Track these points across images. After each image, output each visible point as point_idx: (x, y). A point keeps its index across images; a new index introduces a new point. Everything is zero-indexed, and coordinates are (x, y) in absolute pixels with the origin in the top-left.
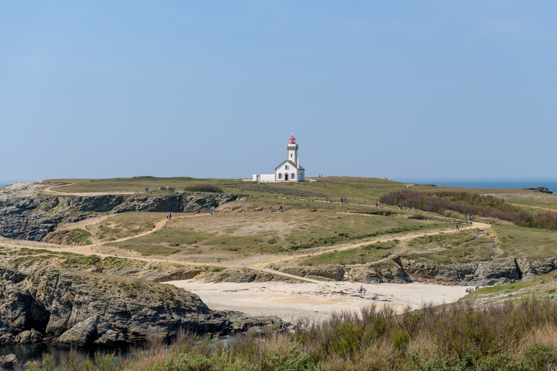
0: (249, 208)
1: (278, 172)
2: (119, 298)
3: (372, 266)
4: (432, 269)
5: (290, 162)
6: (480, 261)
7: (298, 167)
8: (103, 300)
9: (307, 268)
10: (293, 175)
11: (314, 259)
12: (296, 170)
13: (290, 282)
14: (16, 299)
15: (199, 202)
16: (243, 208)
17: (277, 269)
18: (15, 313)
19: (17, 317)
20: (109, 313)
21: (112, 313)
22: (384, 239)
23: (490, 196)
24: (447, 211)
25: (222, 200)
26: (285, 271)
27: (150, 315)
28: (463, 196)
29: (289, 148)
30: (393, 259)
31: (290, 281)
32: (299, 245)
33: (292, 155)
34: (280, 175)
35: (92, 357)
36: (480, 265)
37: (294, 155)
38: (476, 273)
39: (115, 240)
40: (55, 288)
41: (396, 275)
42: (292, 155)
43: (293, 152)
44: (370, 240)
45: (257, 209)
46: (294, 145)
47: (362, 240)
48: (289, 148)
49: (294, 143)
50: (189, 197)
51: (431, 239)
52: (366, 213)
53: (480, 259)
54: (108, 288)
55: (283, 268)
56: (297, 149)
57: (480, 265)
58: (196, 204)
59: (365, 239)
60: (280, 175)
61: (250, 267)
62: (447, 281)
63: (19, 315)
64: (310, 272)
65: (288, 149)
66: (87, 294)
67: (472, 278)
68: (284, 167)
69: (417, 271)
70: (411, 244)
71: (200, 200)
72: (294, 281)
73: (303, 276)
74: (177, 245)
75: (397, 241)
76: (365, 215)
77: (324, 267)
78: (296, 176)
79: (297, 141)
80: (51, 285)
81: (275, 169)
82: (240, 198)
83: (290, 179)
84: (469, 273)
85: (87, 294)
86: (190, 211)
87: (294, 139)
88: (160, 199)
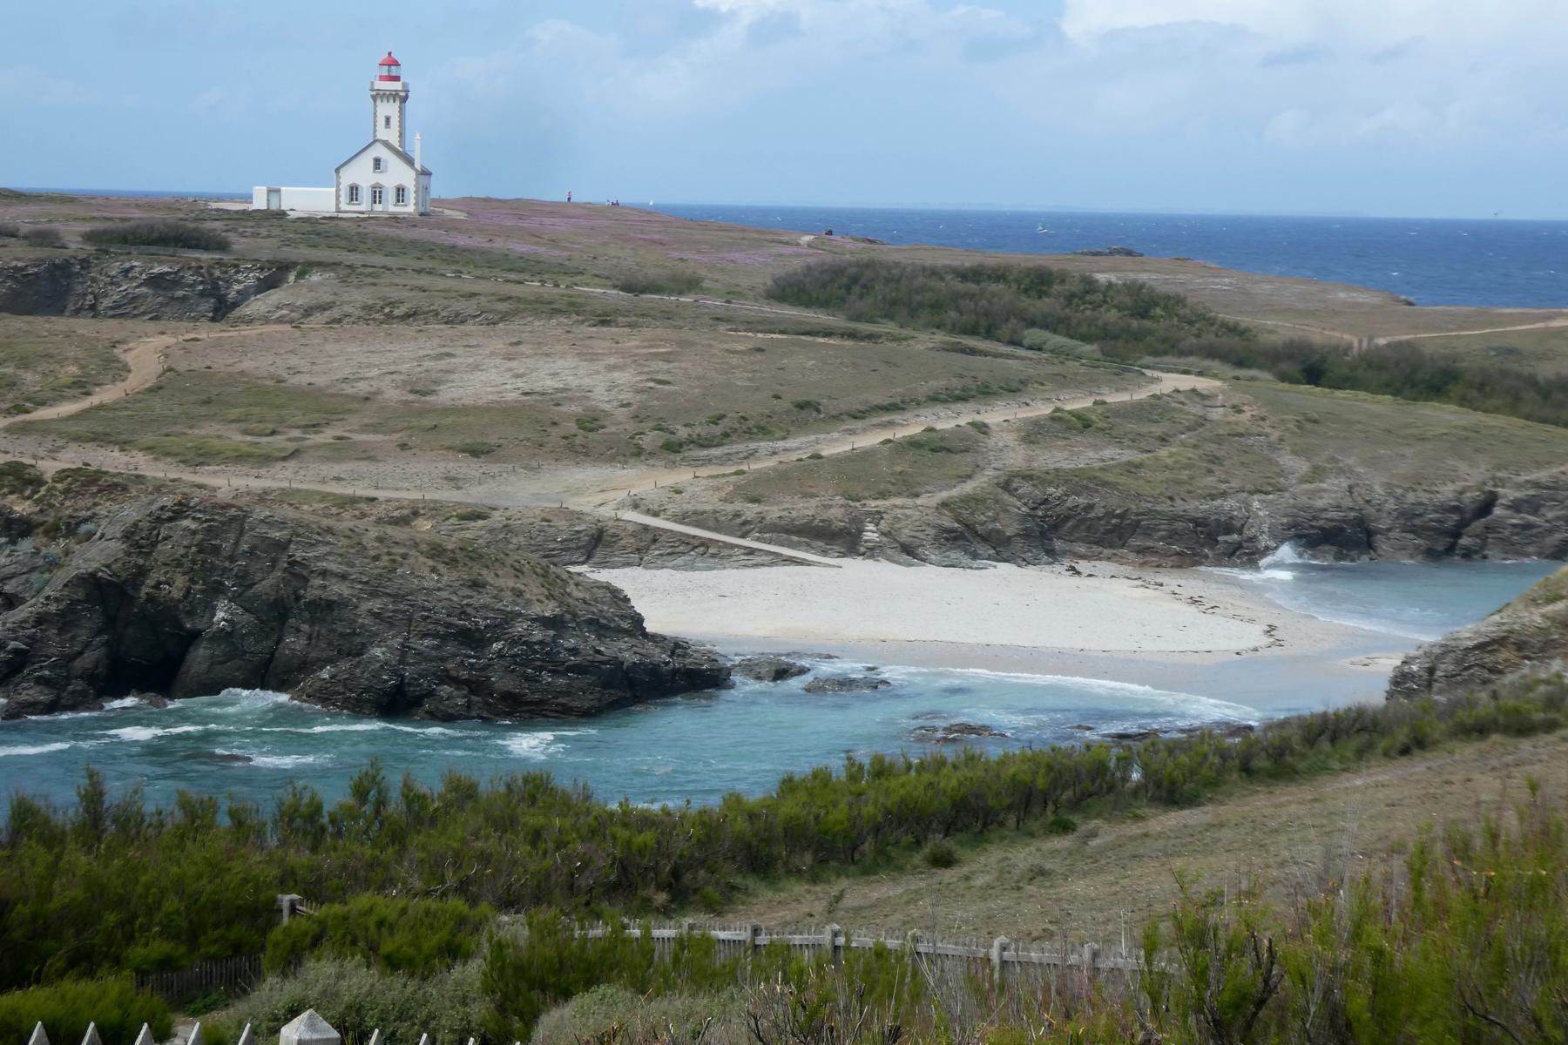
0: (368, 308)
1: (349, 177)
2: (439, 589)
3: (944, 505)
4: (1117, 516)
5: (386, 144)
6: (1251, 493)
7: (417, 166)
8: (395, 596)
9: (751, 511)
10: (400, 192)
11: (762, 479)
12: (413, 174)
13: (713, 556)
14: (81, 595)
15: (156, 281)
16: (348, 309)
17: (656, 514)
18: (73, 638)
19: (80, 653)
20: (424, 636)
21: (435, 636)
22: (949, 420)
23: (1134, 282)
24: (1034, 335)
25: (240, 277)
26: (682, 518)
27: (541, 643)
28: (1040, 281)
29: (378, 96)
30: (998, 484)
31: (712, 550)
32: (683, 433)
33: (388, 120)
34: (354, 191)
35: (93, 797)
36: (1256, 504)
37: (395, 122)
38: (1248, 533)
39: (27, 412)
40: (232, 559)
41: (1018, 535)
42: (388, 120)
43: (391, 109)
44: (891, 424)
45: (397, 312)
46: (397, 86)
47: (866, 422)
48: (378, 96)
49: (397, 78)
50: (115, 268)
51: (1083, 423)
52: (781, 332)
53: (1249, 487)
54: (399, 559)
55: (672, 509)
56: (404, 100)
57: (1256, 504)
58: (144, 290)
59: (875, 420)
60: (354, 191)
61: (575, 504)
62: (1165, 555)
63: (87, 645)
64: (767, 521)
65: (374, 98)
66: (344, 577)
67: (1239, 546)
68: (367, 161)
69: (1070, 524)
70: (1033, 434)
71: (161, 275)
72: (726, 552)
73: (743, 536)
74: (273, 433)
75: (983, 428)
76: (821, 340)
77: (805, 509)
78: (411, 197)
79: (403, 72)
80: (216, 550)
81: (337, 170)
82: (300, 275)
83: (389, 206)
84: (1229, 530)
85: (344, 577)
86: (122, 315)
87: (396, 64)
88: (16, 269)
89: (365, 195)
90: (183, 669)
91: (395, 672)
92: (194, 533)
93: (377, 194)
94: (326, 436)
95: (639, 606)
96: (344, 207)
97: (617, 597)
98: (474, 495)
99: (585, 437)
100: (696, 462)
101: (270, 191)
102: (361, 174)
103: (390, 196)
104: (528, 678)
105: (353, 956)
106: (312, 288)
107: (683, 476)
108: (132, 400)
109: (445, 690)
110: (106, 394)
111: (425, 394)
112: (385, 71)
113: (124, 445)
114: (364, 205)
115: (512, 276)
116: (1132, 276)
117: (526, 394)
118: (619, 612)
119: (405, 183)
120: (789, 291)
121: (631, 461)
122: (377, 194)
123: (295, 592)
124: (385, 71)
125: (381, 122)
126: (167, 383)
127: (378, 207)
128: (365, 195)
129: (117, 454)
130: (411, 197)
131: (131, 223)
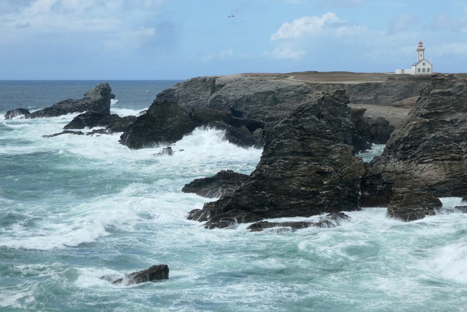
1: (418, 66)
10: (428, 69)
34: (419, 70)
49: (422, 46)
60: (419, 70)
79: (424, 45)
89: (421, 70)
90: (69, 196)
93: (424, 70)
96: (417, 73)
97: (204, 194)
101: (402, 70)
102: (420, 66)
103: (426, 70)
112: (420, 45)
114: (421, 72)
122: (424, 70)
124: (420, 45)
125: (420, 55)
127: (424, 73)
128: (421, 70)
130: (431, 70)
131: (29, 149)
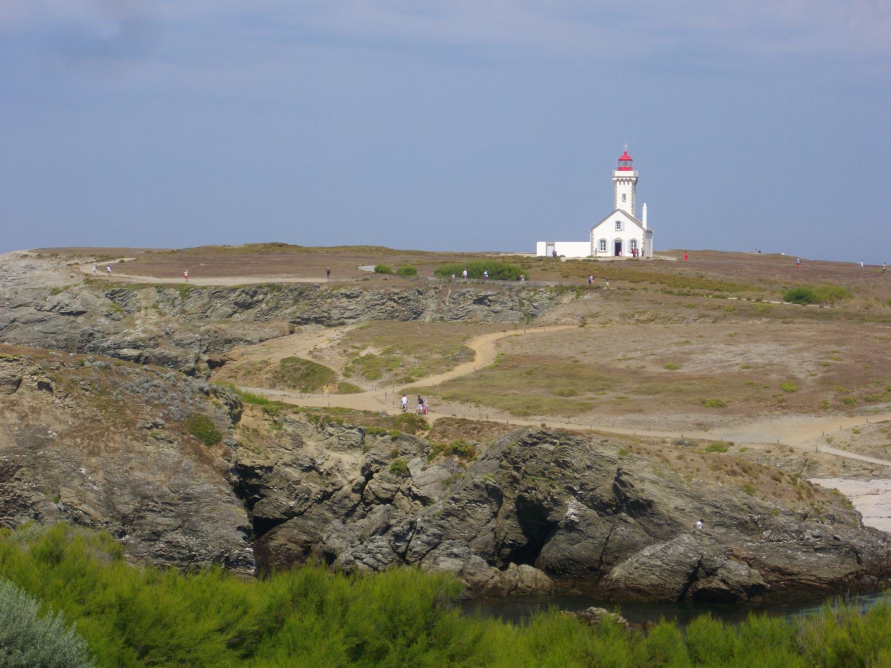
33: (624, 196)
39: (412, 381)
42: (624, 196)
91: (696, 550)
92: (553, 453)
94: (611, 395)
95: (858, 504)
97: (846, 503)
98: (716, 435)
99: (786, 398)
100: (864, 413)
104: (788, 557)
105: (447, 591)
106: (586, 302)
107: (859, 422)
108: (480, 375)
109: (733, 564)
110: (463, 370)
111: (675, 368)
113: (478, 403)
115: (717, 293)
116: (718, 398)
117: (744, 368)
118: (846, 510)
119: (636, 238)
120: (594, 407)
121: (822, 412)
123: (319, 501)
126: (504, 363)
129: (474, 409)
